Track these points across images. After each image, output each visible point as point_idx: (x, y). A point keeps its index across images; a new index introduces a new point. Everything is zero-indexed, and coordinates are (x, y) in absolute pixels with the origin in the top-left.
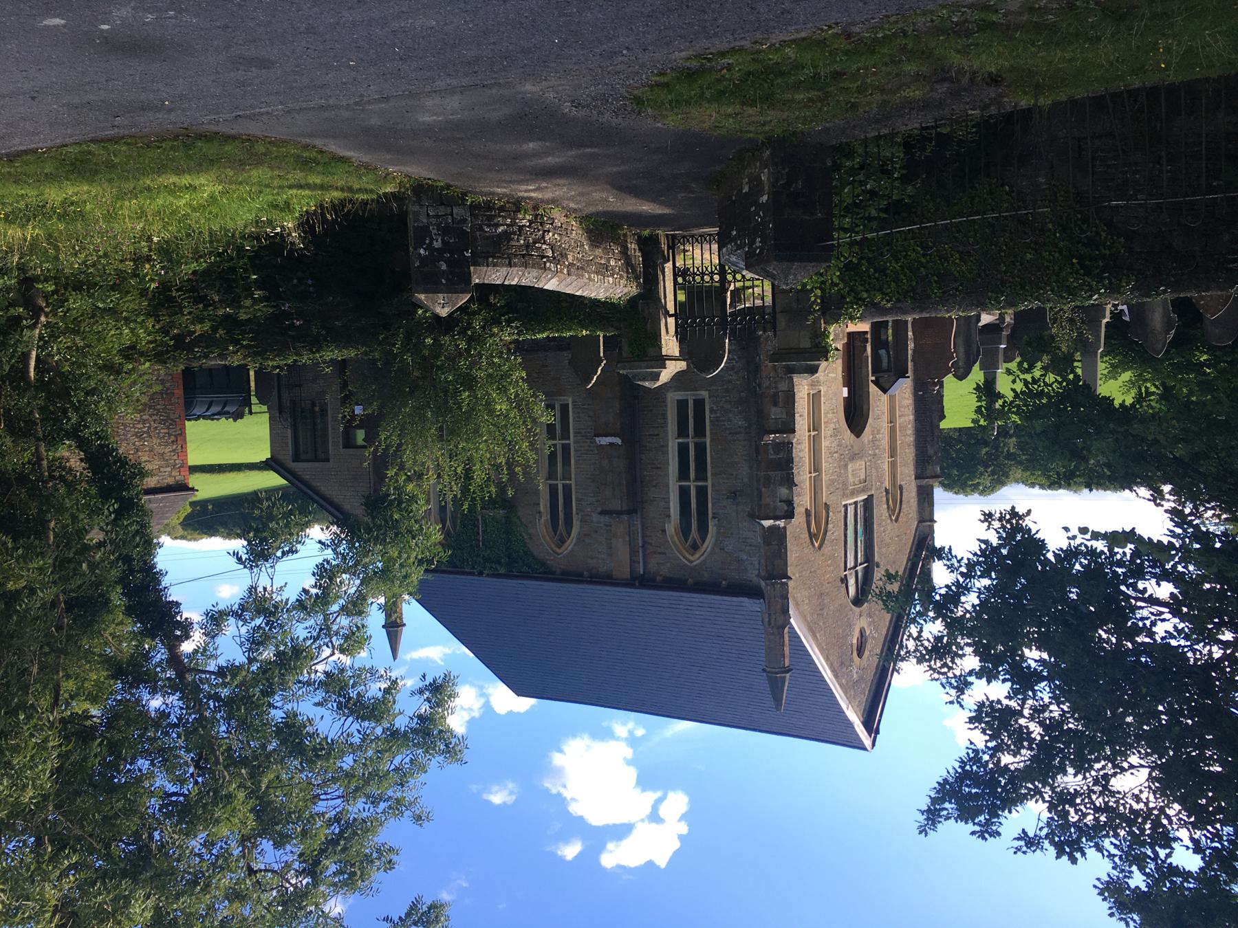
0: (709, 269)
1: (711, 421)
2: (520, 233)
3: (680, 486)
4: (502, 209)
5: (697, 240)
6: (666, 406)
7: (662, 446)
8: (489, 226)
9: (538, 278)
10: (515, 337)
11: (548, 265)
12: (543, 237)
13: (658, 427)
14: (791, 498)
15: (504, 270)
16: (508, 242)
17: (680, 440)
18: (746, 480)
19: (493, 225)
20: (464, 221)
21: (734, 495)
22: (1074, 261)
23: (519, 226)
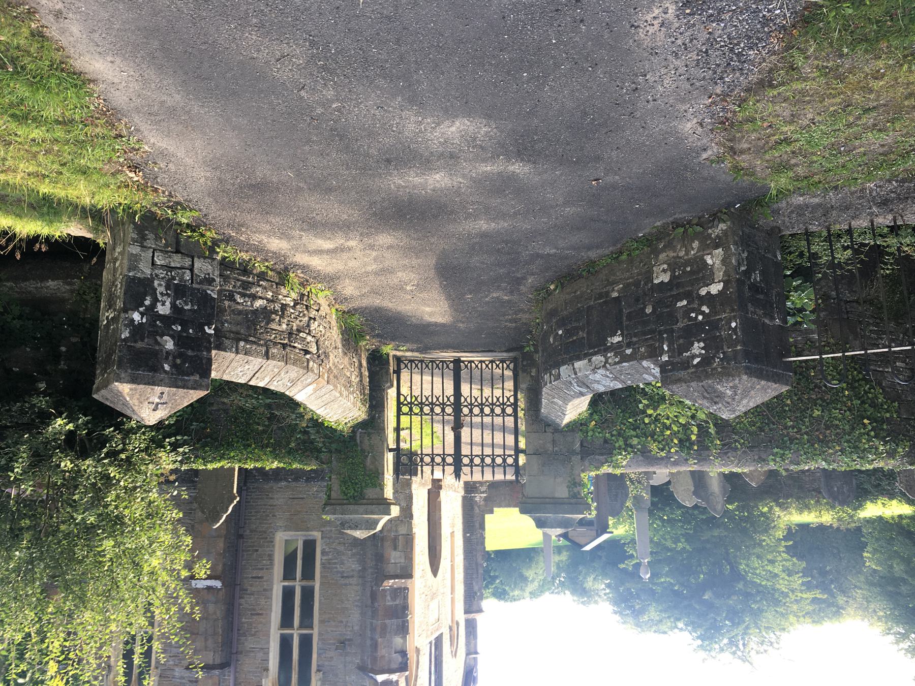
0: (441, 400)
1: (322, 564)
2: (283, 313)
3: (281, 635)
4: (262, 276)
5: (437, 366)
6: (273, 546)
7: (265, 590)
8: (243, 295)
9: (294, 382)
10: (177, 465)
11: (311, 363)
12: (308, 326)
13: (262, 569)
14: (404, 649)
15: (256, 362)
16: (268, 323)
17: (286, 584)
18: (356, 628)
19: (250, 296)
20: (210, 281)
21: (343, 644)
22: (866, 421)
23: (282, 304)
